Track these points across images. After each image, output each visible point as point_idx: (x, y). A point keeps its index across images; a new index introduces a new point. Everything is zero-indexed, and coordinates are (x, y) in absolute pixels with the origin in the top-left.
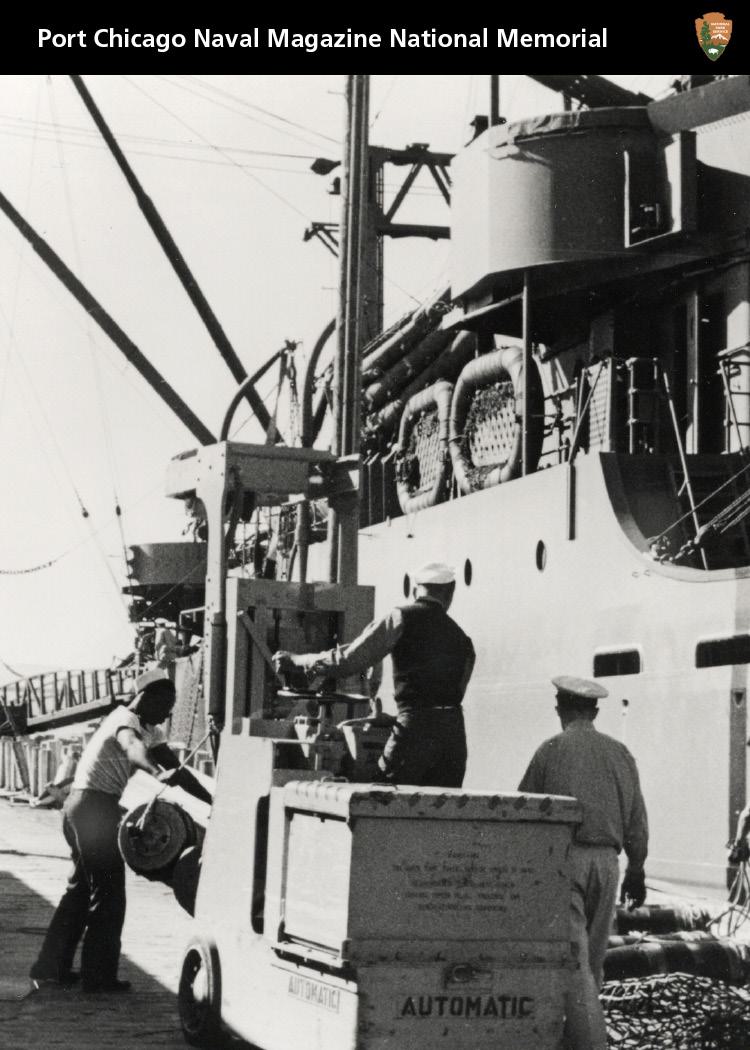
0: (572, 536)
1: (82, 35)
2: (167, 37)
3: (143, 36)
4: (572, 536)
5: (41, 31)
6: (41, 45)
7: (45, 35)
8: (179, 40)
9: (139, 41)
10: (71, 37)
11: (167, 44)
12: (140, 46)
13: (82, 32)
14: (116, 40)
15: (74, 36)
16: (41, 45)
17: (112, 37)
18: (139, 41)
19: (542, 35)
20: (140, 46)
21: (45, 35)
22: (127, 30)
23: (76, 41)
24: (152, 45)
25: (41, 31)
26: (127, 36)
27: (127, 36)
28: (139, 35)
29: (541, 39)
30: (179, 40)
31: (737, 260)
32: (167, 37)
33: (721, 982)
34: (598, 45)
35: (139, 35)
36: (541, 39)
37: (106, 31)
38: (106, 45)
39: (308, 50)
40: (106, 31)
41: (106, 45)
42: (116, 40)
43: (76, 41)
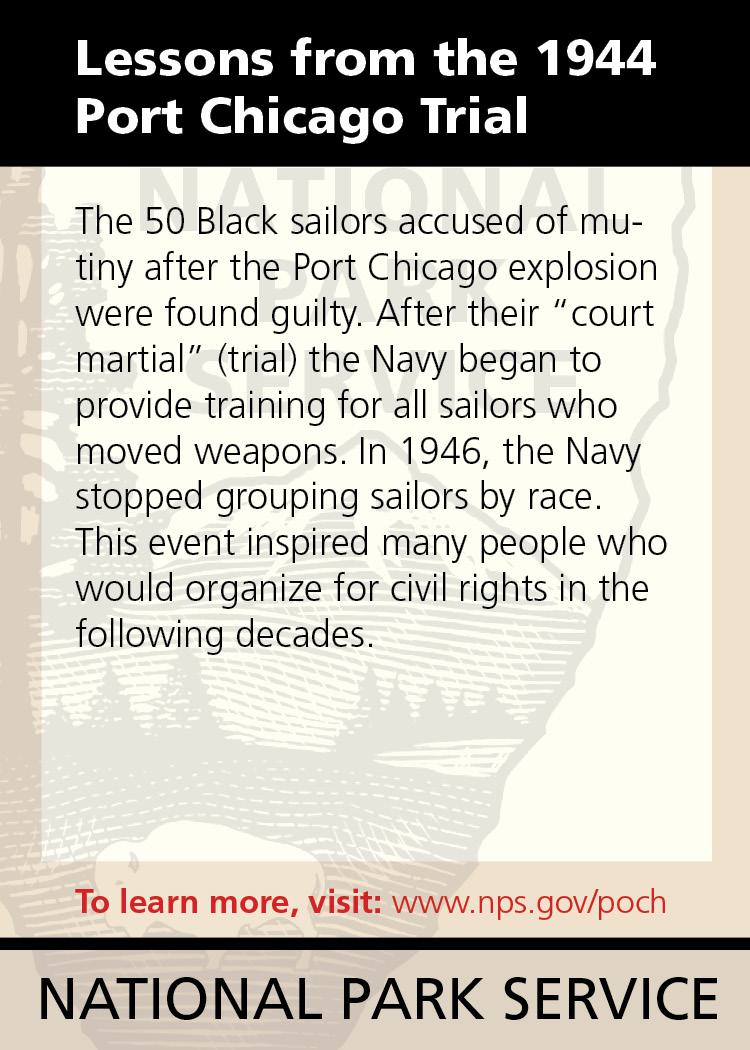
0: (513, 490)
1: (172, 111)
2: (364, 113)
3: (309, 111)
4: (513, 490)
5: (83, 103)
6: (82, 128)
7: (91, 110)
8: (388, 121)
9: (300, 121)
10: (148, 114)
11: (363, 126)
12: (303, 130)
13: (172, 104)
14: (249, 120)
15: (157, 111)
16: (82, 128)
17: (240, 114)
18: (300, 121)
19: (387, 53)
20: (303, 130)
21: (91, 110)
22: (274, 99)
23: (159, 122)
24: (330, 128)
25: (83, 103)
26: (274, 113)
27: (274, 113)
28: (302, 111)
29: (383, 62)
30: (388, 121)
31: (164, 819)
32: (364, 113)
33: (48, 723)
34: (506, 128)
35: (302, 111)
36: (383, 62)
37: (227, 101)
38: (227, 130)
39: (347, 140)
40: (227, 101)
41: (227, 130)
42: (249, 120)
43: (159, 122)
